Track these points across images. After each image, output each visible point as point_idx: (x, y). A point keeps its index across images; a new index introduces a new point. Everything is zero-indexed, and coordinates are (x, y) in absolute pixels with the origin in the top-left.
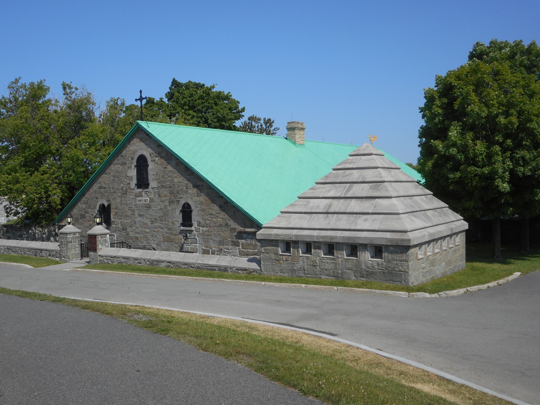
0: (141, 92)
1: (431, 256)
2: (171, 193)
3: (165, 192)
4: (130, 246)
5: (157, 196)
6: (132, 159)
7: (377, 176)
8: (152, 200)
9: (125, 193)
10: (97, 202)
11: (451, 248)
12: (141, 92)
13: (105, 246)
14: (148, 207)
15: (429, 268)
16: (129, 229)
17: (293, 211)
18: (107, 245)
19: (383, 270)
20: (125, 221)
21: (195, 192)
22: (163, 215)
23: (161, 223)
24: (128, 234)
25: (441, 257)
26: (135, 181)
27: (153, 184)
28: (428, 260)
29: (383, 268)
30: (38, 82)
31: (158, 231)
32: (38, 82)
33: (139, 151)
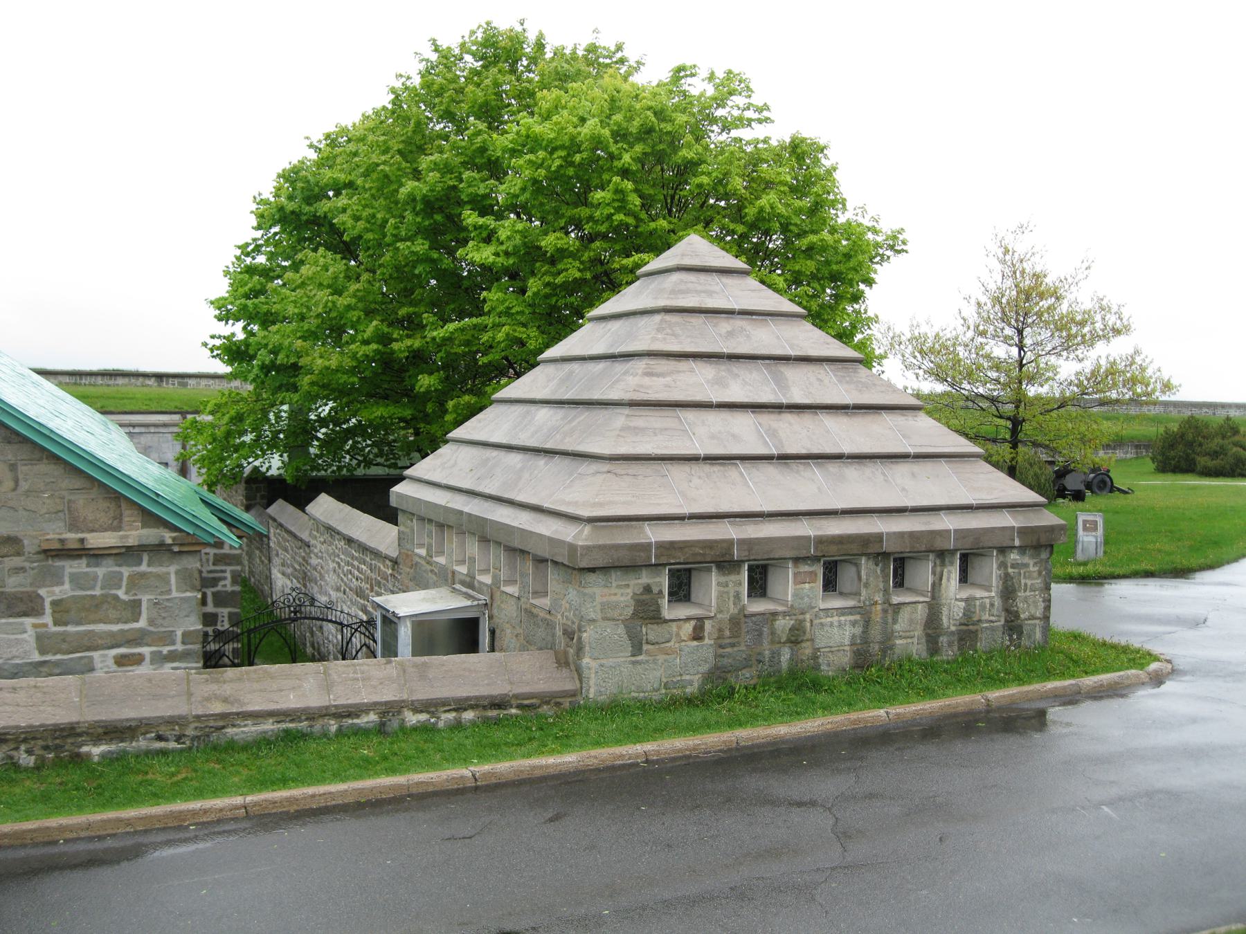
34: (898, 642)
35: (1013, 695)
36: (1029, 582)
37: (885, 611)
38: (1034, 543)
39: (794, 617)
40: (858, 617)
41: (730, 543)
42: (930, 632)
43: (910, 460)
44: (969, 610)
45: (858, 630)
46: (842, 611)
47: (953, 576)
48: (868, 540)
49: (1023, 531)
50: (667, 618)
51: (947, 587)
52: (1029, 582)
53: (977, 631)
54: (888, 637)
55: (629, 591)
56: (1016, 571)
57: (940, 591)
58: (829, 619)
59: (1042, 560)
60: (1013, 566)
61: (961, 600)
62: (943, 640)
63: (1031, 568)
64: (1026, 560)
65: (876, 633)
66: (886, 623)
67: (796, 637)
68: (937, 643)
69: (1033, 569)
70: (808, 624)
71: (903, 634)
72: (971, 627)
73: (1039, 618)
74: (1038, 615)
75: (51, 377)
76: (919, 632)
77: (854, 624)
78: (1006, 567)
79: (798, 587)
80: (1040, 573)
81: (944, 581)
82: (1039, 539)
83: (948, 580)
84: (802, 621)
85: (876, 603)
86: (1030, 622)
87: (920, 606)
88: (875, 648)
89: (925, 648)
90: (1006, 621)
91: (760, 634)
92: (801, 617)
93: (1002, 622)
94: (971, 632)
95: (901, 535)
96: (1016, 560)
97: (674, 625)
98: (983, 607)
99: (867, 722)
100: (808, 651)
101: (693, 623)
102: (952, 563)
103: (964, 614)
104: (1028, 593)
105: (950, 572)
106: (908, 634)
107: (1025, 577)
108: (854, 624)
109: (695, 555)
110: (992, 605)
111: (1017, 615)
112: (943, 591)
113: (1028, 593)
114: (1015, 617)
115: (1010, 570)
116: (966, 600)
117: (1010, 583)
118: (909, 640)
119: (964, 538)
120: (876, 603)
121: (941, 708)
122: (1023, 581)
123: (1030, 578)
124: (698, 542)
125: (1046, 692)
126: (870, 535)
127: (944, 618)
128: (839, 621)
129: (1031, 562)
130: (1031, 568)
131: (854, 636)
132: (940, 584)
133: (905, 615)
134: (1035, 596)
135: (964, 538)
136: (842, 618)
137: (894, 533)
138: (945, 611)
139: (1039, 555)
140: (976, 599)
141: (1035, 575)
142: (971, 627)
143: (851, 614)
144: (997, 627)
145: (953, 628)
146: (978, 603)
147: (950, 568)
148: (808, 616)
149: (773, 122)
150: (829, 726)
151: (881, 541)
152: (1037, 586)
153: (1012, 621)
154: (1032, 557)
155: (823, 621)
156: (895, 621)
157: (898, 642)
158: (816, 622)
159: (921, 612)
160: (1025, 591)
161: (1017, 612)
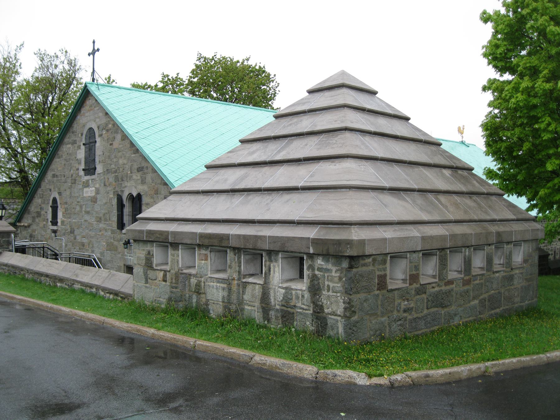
0: (94, 42)
1: (434, 285)
2: (117, 179)
3: (111, 178)
4: (56, 255)
5: (103, 185)
6: (82, 135)
7: (336, 121)
8: (98, 191)
9: (74, 182)
10: (50, 196)
11: (497, 272)
12: (94, 42)
13: (8, 250)
14: (94, 200)
15: (426, 311)
16: (76, 232)
17: (189, 189)
18: (11, 248)
19: (303, 309)
20: (74, 221)
21: (139, 177)
22: (107, 212)
23: (105, 224)
24: (75, 239)
25: (466, 288)
26: (83, 166)
27: (100, 169)
28: (425, 293)
29: (303, 306)
30: (81, 78)
31: (102, 234)
32: (81, 78)
33: (88, 124)
34: (246, 307)
35: (207, 346)
36: (331, 285)
37: (238, 285)
38: (324, 253)
39: (197, 279)
40: (225, 286)
41: (167, 232)
42: (264, 305)
43: (300, 191)
44: (286, 296)
45: (226, 294)
46: (219, 280)
47: (277, 269)
48: (222, 238)
49: (316, 242)
50: (155, 268)
51: (273, 277)
52: (331, 285)
53: (293, 313)
54: (241, 302)
55: (144, 252)
56: (322, 273)
57: (269, 278)
58: (212, 284)
59: (342, 268)
60: (319, 269)
61: (283, 288)
62: (272, 313)
63: (333, 274)
64: (330, 266)
65: (234, 297)
66: (239, 293)
67: (198, 291)
68: (268, 315)
69: (335, 274)
70: (203, 284)
71: (249, 303)
72: (289, 309)
73: (339, 316)
74: (339, 313)
75: (459, 165)
76: (257, 304)
77: (224, 289)
78: (313, 270)
79: (200, 262)
80: (340, 279)
81: (272, 272)
82: (328, 250)
83: (274, 273)
84: (200, 282)
85: (234, 279)
86: (333, 317)
87: (257, 287)
88: (233, 307)
89: (262, 316)
90: (314, 311)
91: (185, 285)
92: (200, 279)
93: (311, 312)
94: (289, 313)
95: (239, 236)
96: (321, 265)
97: (157, 272)
98: (297, 298)
99: (142, 332)
100: (204, 300)
101: (163, 272)
102: (276, 261)
103: (283, 298)
104: (330, 293)
105: (274, 266)
106: (251, 304)
107: (328, 280)
108: (224, 289)
109: (157, 237)
110: (303, 296)
111: (322, 308)
112: (271, 280)
113: (330, 293)
114: (320, 309)
115: (317, 272)
116: (286, 288)
117: (316, 282)
118: (253, 308)
119: (275, 242)
120: (234, 279)
121: (171, 338)
122: (326, 283)
123: (331, 281)
124: (158, 231)
125: (227, 353)
126: (224, 235)
127: (272, 298)
128: (217, 286)
129: (334, 269)
130: (333, 274)
131: (223, 297)
132: (270, 274)
133: (249, 288)
134: (337, 297)
135: (275, 242)
136: (218, 285)
137: (235, 235)
138: (272, 294)
139: (340, 264)
140: (292, 289)
141: (336, 279)
142: (289, 309)
143: (221, 283)
144: (307, 314)
145: (278, 307)
146: (294, 292)
147: (275, 264)
148: (203, 279)
149: (94, 40)
150: (129, 329)
151: (229, 239)
152: (338, 289)
153: (318, 313)
154: (334, 264)
155: (209, 284)
156: (244, 293)
157: (246, 307)
158: (207, 284)
159: (258, 291)
160: (328, 291)
161: (322, 306)
